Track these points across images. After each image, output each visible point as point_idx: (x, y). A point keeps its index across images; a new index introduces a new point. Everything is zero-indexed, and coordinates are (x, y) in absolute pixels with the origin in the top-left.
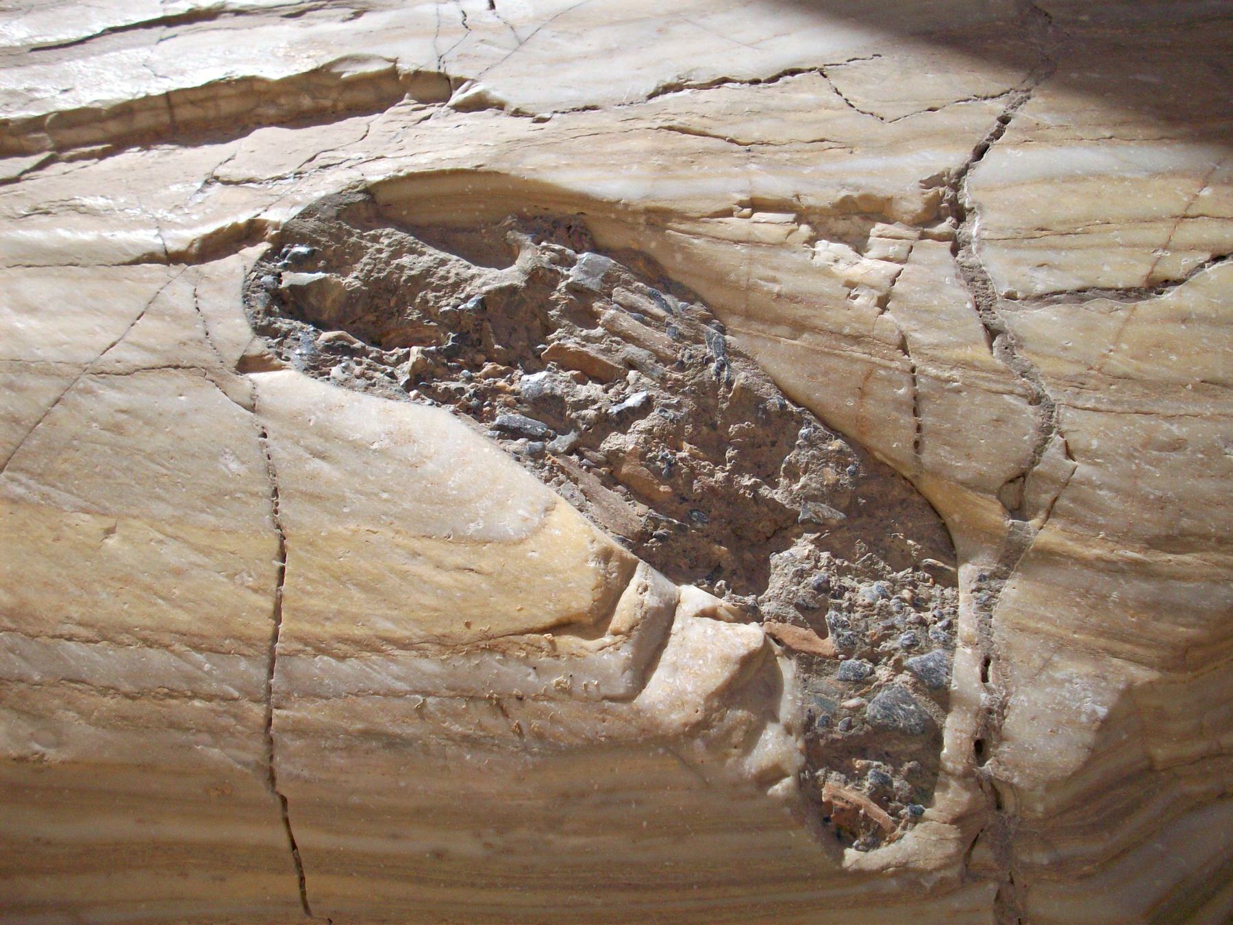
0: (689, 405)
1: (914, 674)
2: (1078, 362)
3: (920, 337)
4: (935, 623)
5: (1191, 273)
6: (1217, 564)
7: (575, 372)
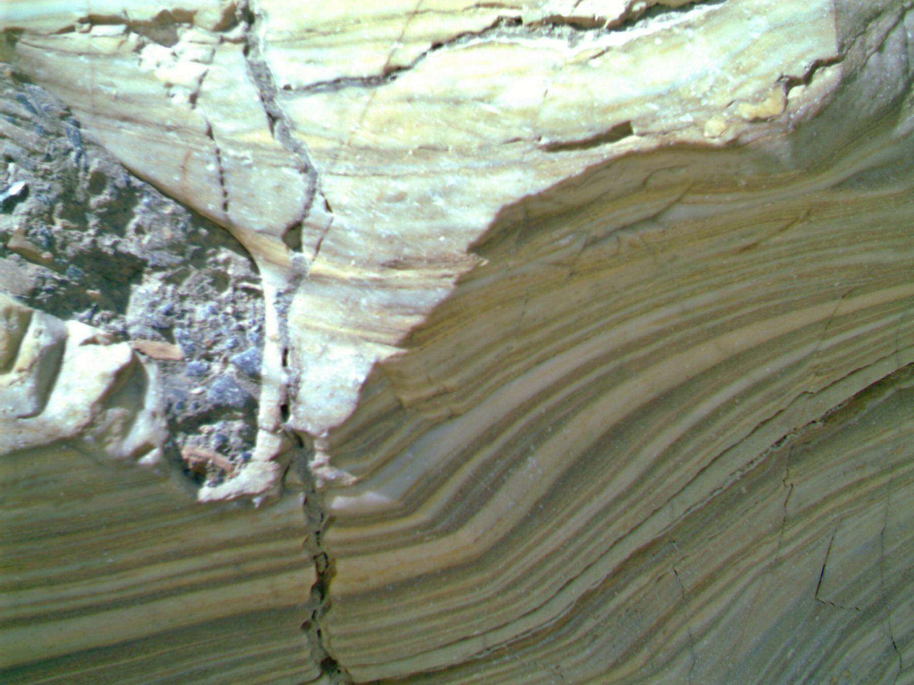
0: (58, 188)
1: (237, 366)
2: (333, 139)
3: (223, 126)
4: (250, 327)
5: (417, 60)
6: (429, 277)
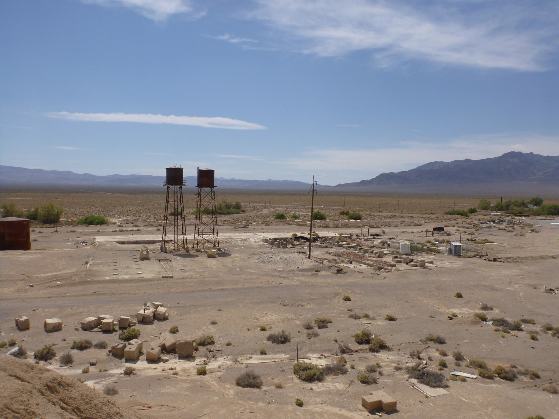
7: (112, 316)
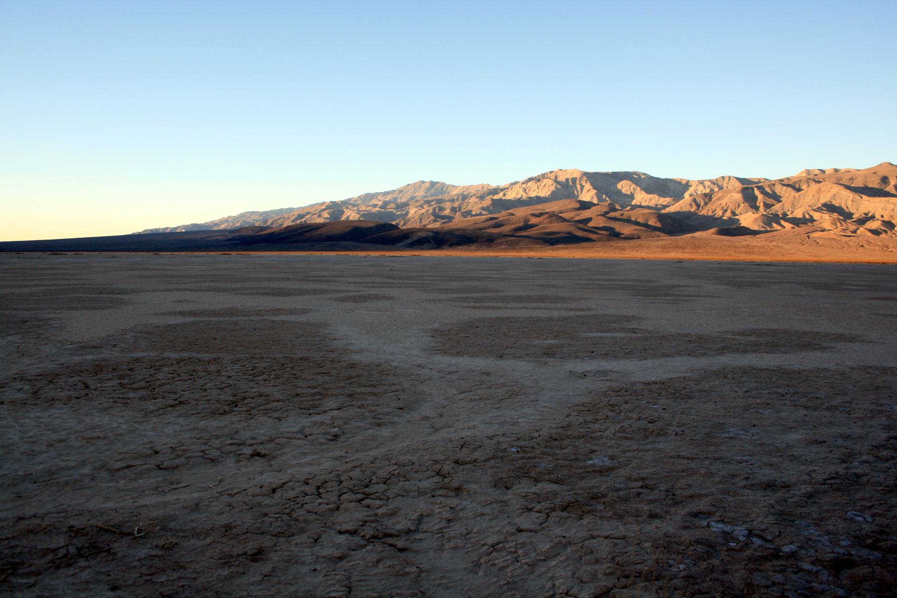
6: (58, 478)
